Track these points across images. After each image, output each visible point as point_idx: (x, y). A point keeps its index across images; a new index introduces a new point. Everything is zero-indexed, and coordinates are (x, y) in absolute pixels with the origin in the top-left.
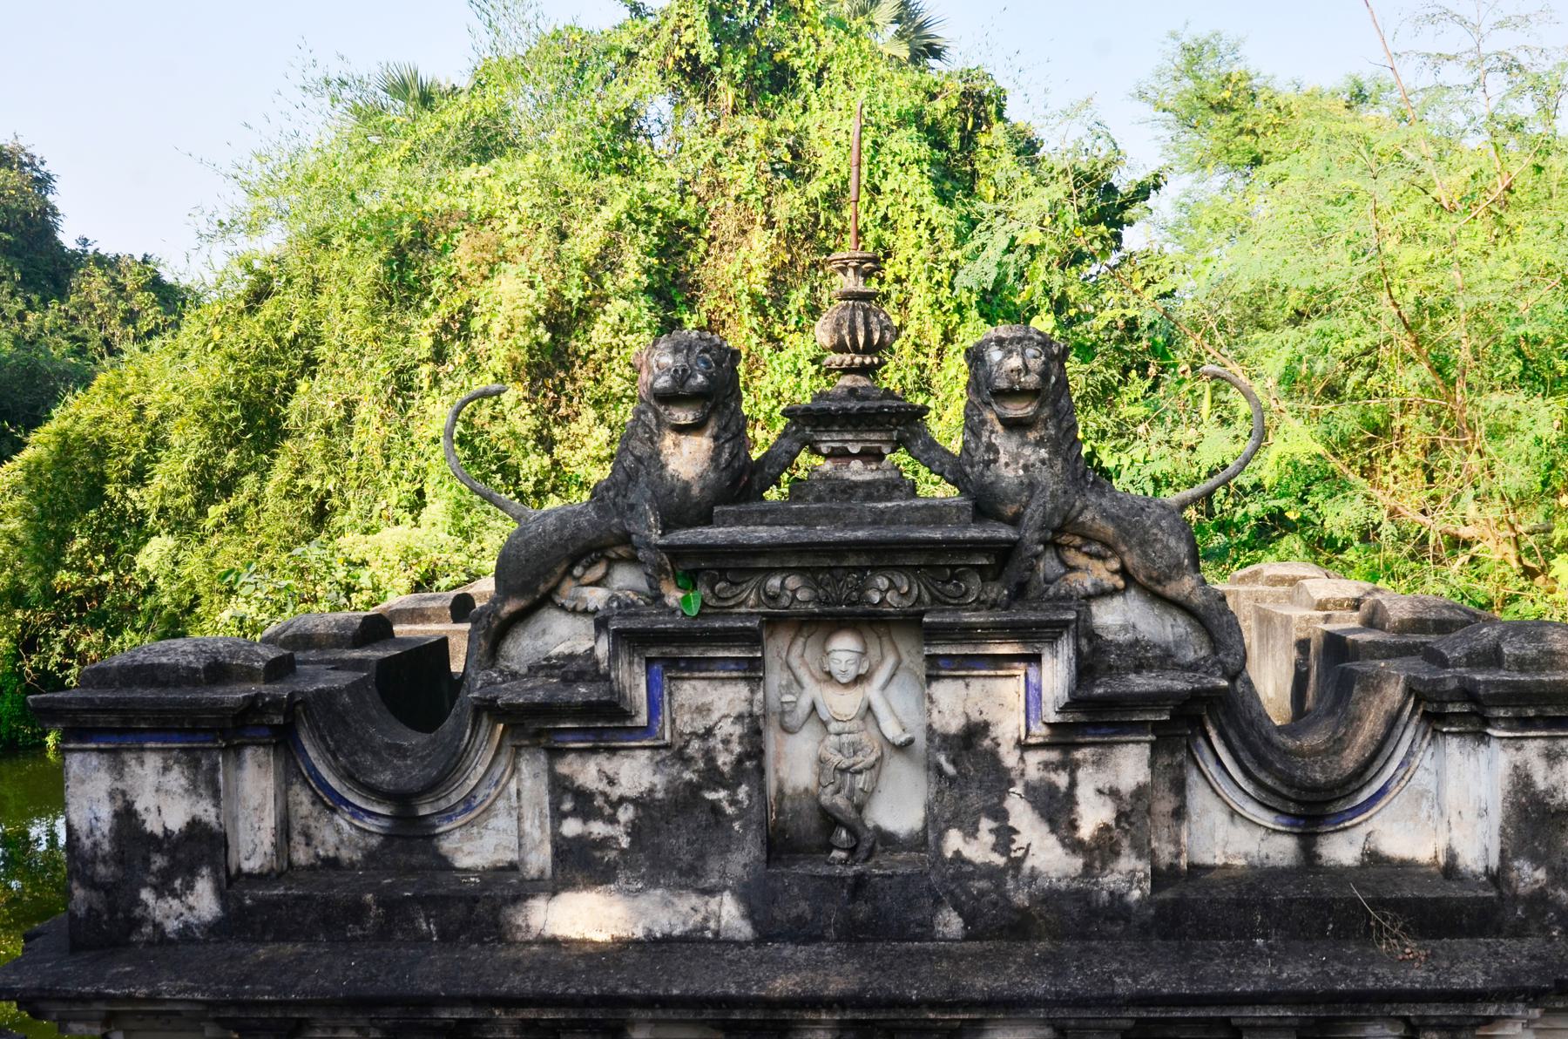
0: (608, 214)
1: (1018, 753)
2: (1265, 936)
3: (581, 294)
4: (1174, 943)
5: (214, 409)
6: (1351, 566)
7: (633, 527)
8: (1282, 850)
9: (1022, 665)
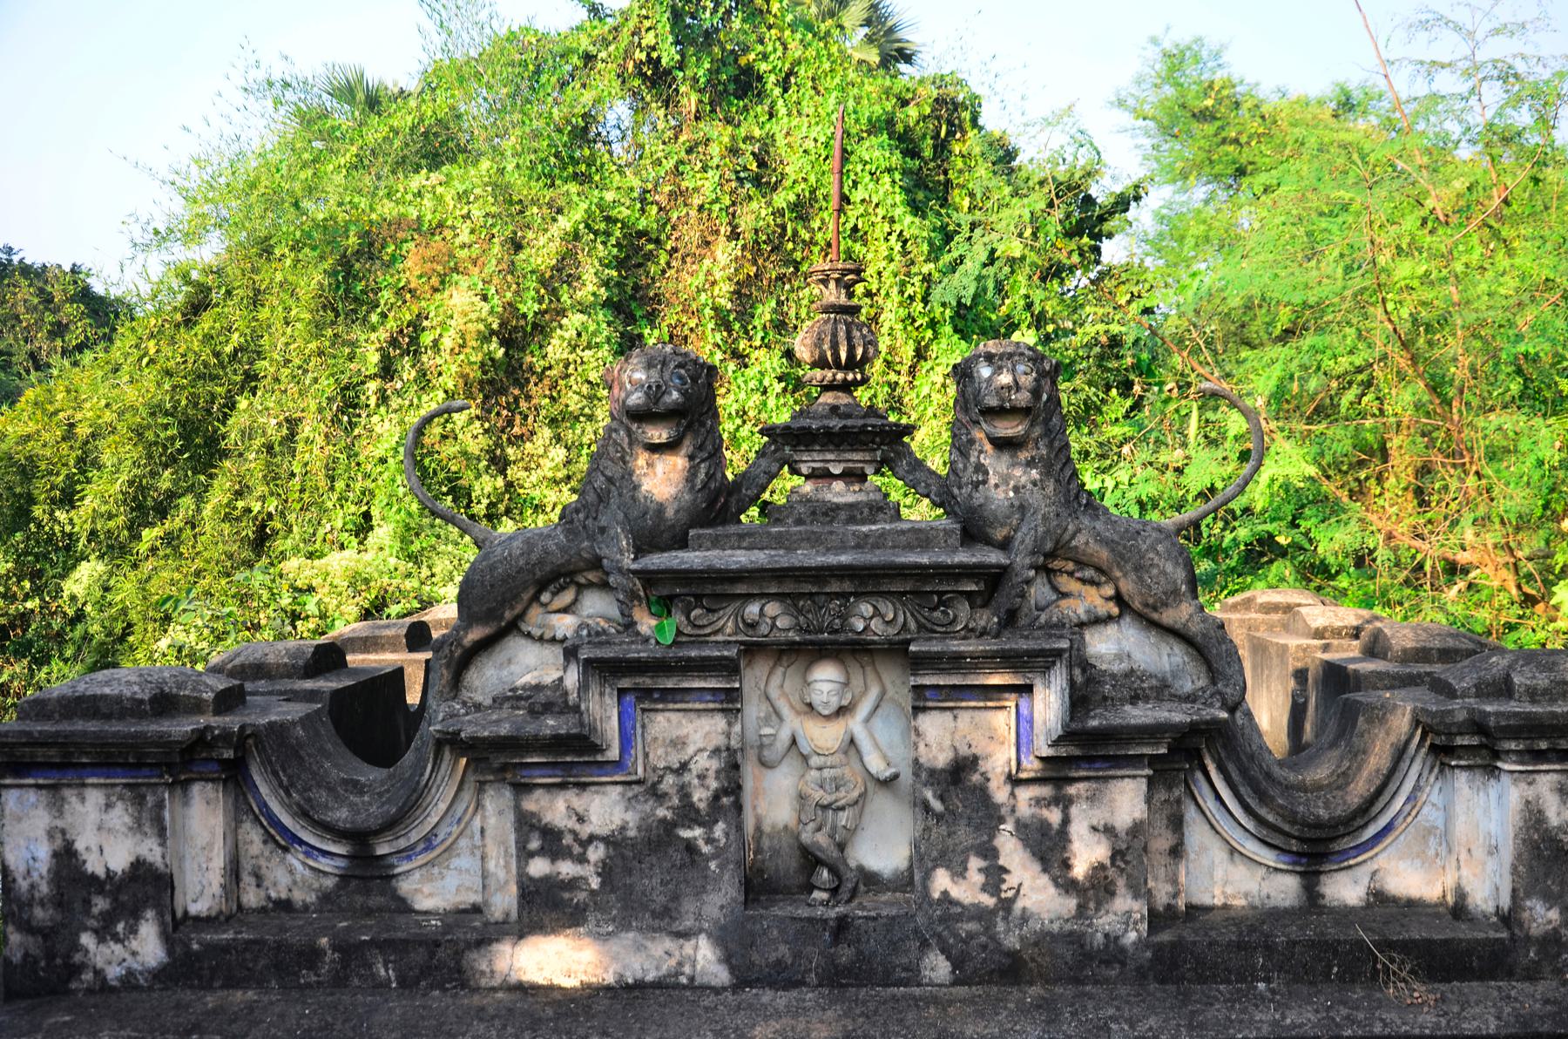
0: (565, 223)
1: (1008, 788)
2: (1267, 980)
3: (536, 307)
4: (1172, 988)
5: (149, 427)
6: (1344, 593)
7: (604, 552)
8: (1284, 889)
9: (1013, 696)
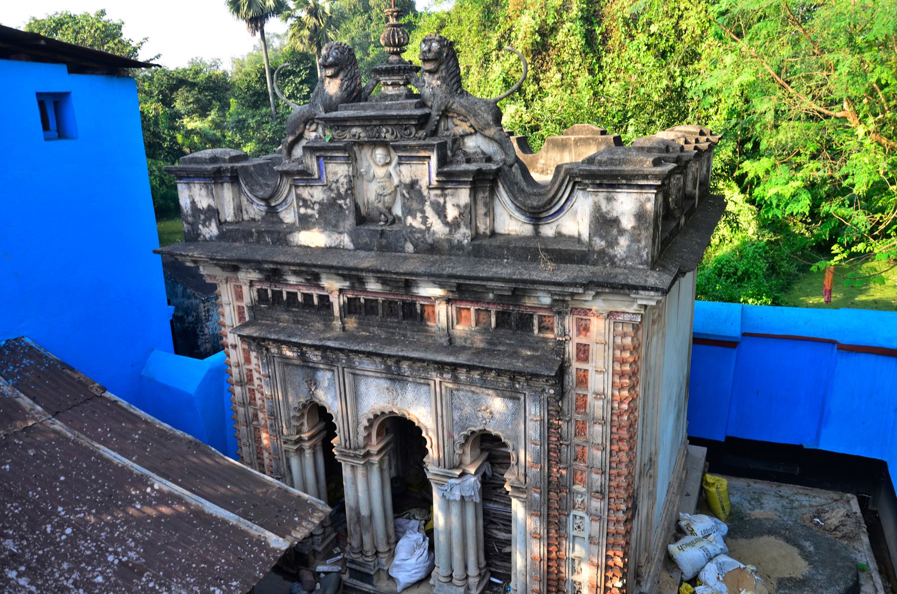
8: (526, 229)
